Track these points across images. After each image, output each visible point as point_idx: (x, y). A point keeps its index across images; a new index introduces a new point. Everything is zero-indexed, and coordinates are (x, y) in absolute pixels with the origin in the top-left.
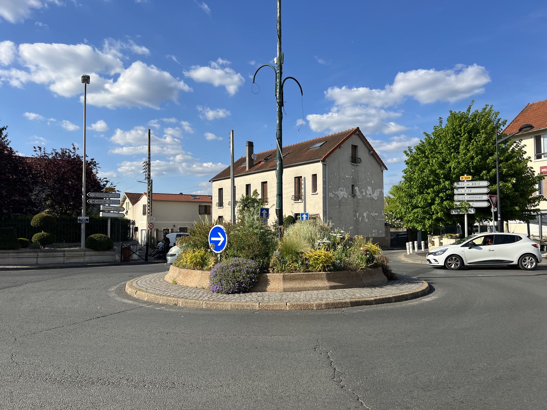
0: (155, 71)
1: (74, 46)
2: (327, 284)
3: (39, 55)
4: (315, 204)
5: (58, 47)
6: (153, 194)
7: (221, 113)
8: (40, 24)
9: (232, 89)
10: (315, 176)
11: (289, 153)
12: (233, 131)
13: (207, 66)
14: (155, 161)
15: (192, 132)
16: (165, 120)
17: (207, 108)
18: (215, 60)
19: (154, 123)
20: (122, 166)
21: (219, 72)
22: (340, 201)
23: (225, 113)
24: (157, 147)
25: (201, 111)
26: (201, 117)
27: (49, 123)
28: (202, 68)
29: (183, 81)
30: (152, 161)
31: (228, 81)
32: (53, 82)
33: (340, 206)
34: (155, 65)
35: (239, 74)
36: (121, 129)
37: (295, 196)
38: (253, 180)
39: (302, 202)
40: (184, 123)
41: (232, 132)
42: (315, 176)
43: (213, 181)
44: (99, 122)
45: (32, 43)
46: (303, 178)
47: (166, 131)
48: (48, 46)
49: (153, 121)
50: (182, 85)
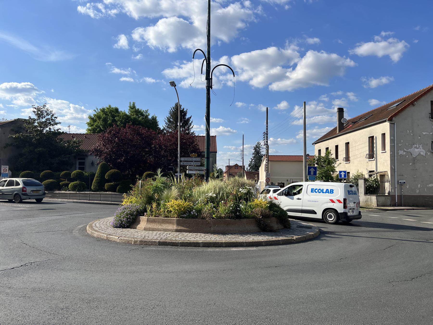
0: (324, 55)
1: (265, 49)
2: (175, 227)
3: (243, 62)
4: (384, 161)
5: (255, 53)
6: (269, 156)
7: (384, 80)
8: (244, 39)
9: (396, 57)
10: (384, 135)
11: (372, 115)
12: (305, 102)
13: (371, 42)
14: (325, 128)
15: (357, 100)
16: (333, 94)
17: (371, 78)
18: (378, 34)
19: (324, 98)
20: (300, 134)
21: (383, 44)
22: (414, 159)
23: (388, 79)
24: (327, 116)
25: (365, 82)
26: (365, 86)
27: (250, 108)
28: (366, 44)
29: (349, 58)
30: (308, 130)
31: (392, 49)
32: (251, 79)
33: (414, 163)
34: (324, 50)
35: (403, 41)
36: (298, 105)
37: (369, 155)
38: (340, 141)
39: (375, 160)
40: (349, 94)
41: (304, 103)
42: (384, 135)
43: (316, 144)
44: (282, 102)
45: (239, 55)
46: (375, 138)
47: (334, 103)
48: (249, 54)
49: (323, 96)
50: (349, 63)
